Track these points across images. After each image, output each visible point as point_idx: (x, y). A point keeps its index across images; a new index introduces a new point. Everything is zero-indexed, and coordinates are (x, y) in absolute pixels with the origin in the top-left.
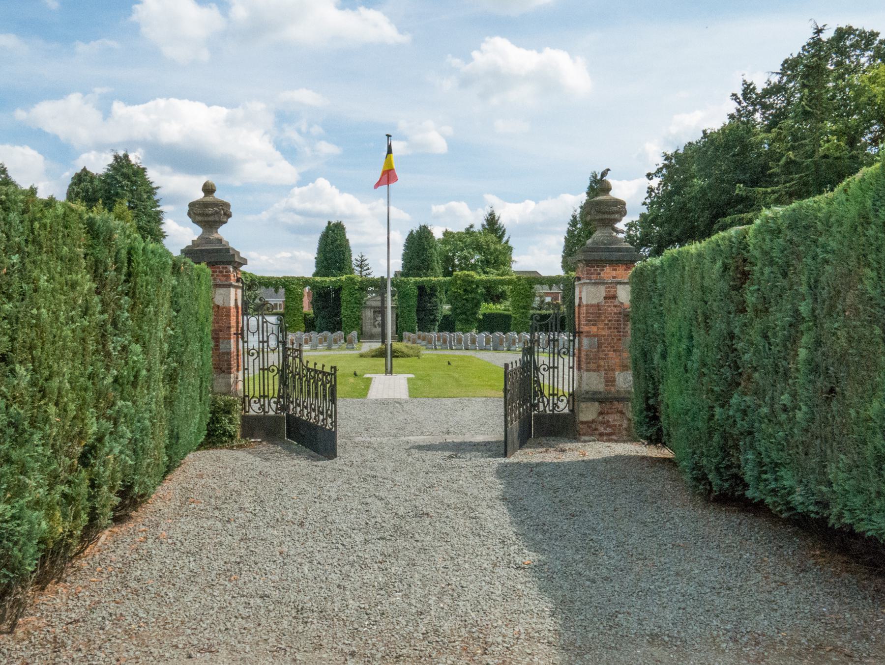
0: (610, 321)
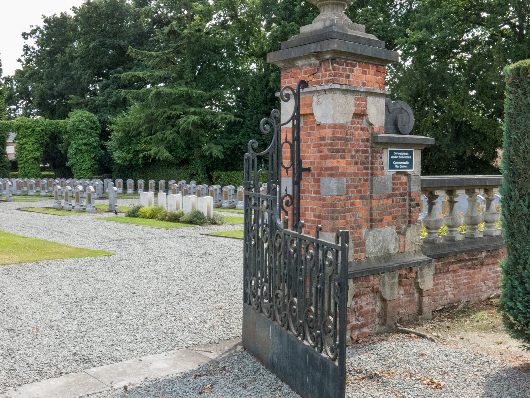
0: (357, 151)
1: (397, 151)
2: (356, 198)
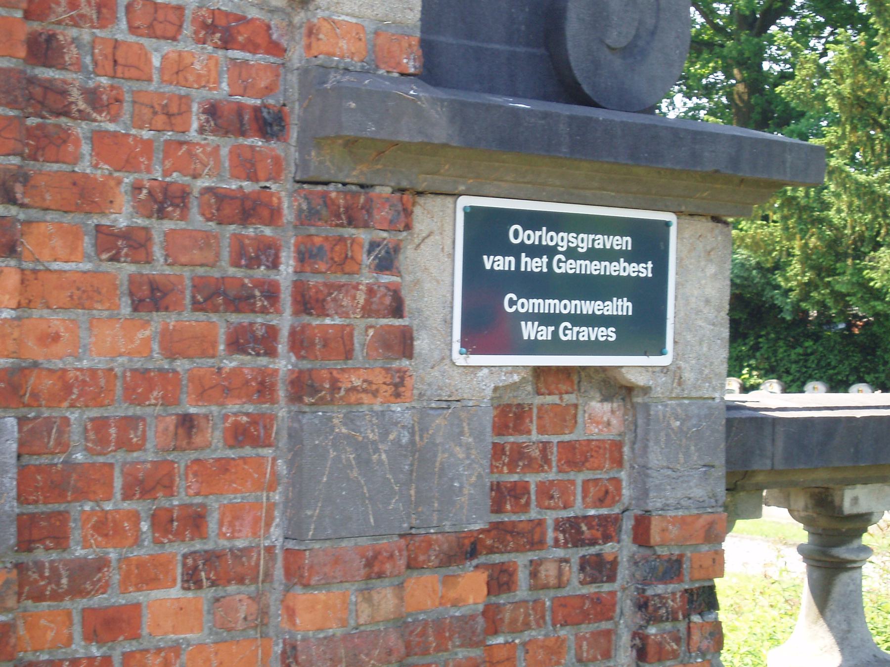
0: (165, 201)
1: (533, 221)
2: (147, 575)
